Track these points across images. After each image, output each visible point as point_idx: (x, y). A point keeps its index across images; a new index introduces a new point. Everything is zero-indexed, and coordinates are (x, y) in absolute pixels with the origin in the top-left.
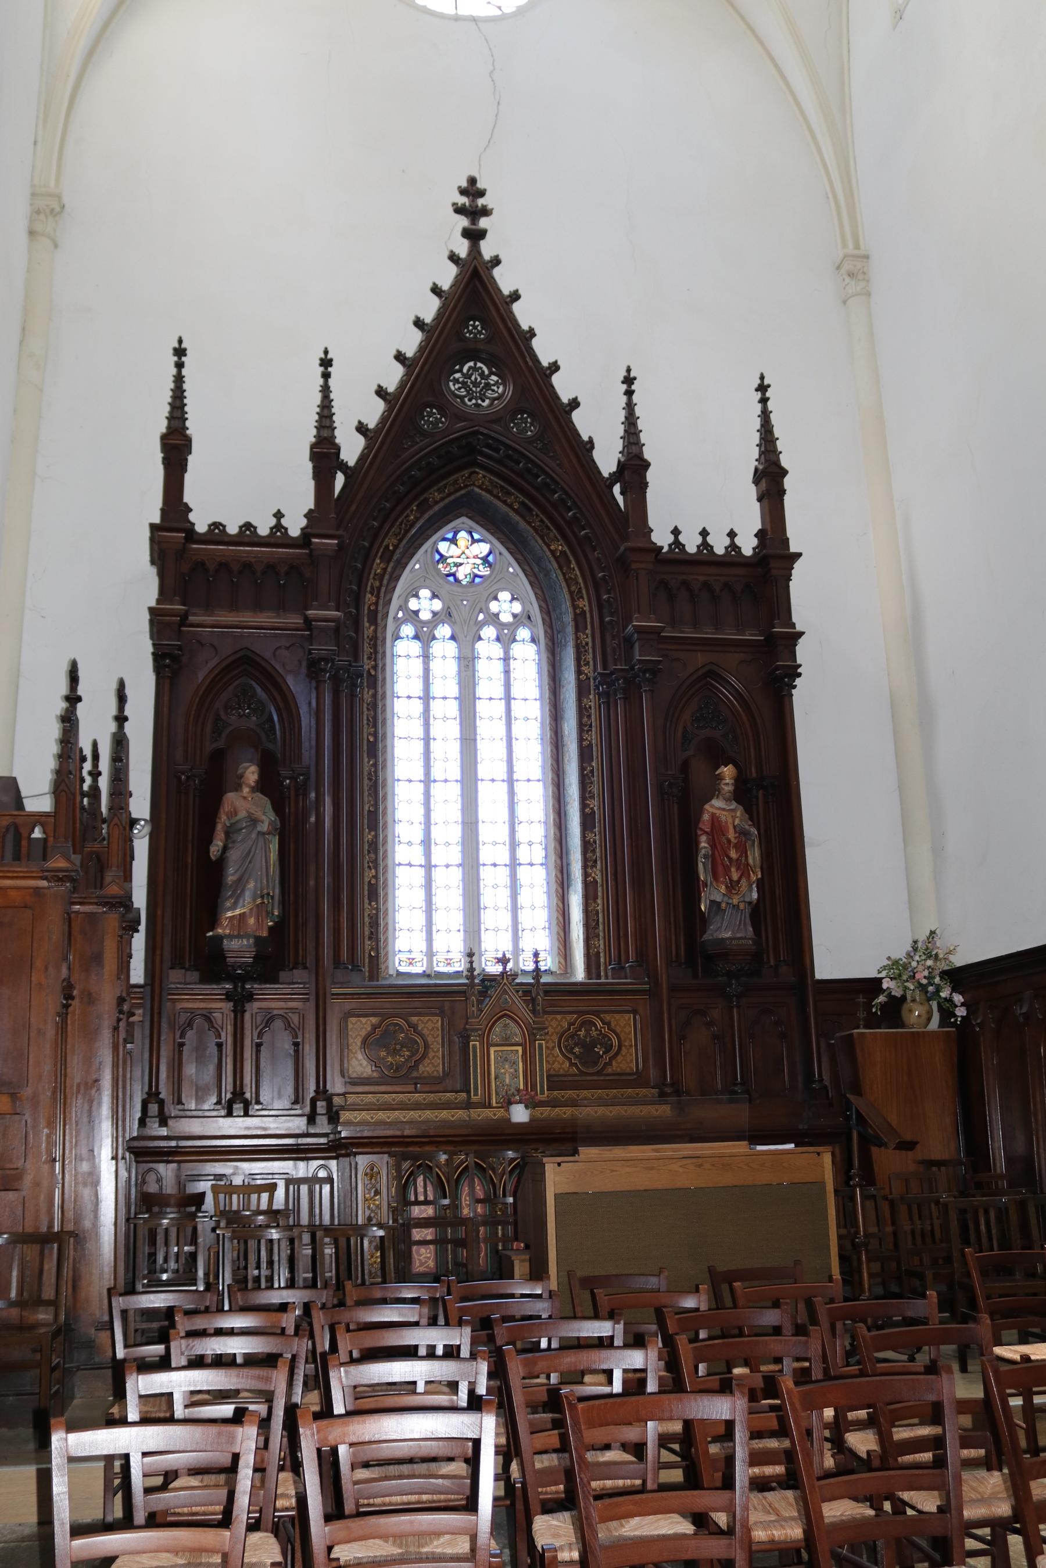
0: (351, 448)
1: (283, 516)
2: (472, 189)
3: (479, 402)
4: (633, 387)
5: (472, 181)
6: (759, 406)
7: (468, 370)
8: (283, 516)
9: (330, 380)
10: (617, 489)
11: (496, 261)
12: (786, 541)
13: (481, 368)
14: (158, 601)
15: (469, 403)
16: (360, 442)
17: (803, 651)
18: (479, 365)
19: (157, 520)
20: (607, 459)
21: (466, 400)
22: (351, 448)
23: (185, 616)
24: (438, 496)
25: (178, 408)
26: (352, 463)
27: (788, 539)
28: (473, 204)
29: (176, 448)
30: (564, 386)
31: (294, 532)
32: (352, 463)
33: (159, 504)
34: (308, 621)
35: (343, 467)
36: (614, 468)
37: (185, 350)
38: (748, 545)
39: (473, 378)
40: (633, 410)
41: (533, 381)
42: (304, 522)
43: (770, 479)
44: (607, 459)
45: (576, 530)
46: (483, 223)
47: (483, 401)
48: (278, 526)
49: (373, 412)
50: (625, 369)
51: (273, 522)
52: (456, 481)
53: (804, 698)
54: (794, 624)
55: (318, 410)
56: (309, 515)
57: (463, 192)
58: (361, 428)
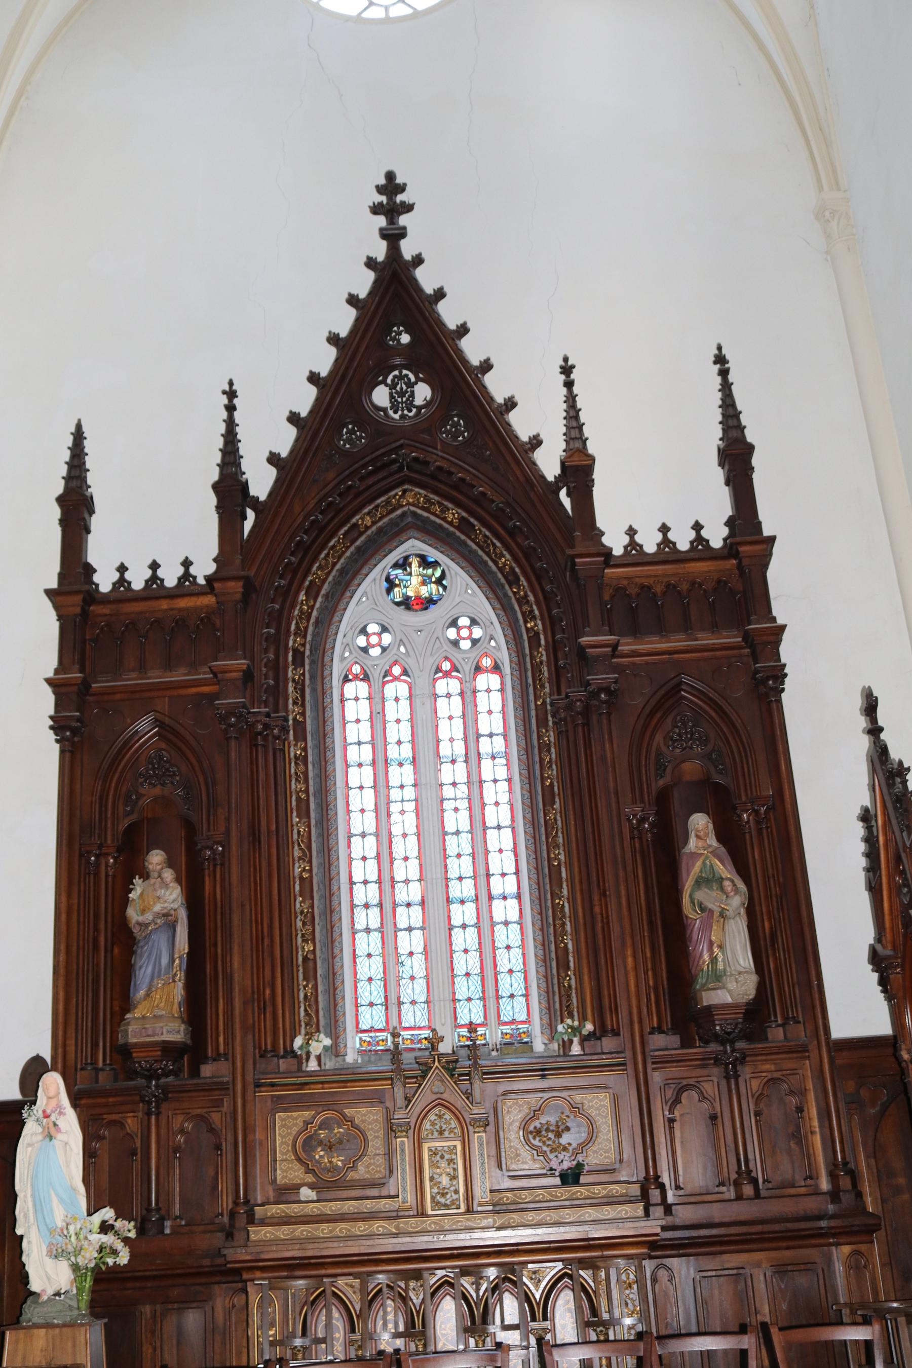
0: (261, 481)
1: (127, 569)
2: (391, 186)
3: (406, 412)
4: (572, 376)
5: (390, 176)
6: (564, 391)
7: (393, 381)
8: (127, 569)
9: (236, 413)
10: (563, 494)
11: (418, 260)
12: (758, 526)
13: (407, 376)
14: (57, 672)
15: (411, 414)
16: (271, 473)
17: (787, 651)
18: (405, 372)
19: (54, 584)
20: (549, 462)
21: (391, 412)
22: (261, 481)
23: (615, 647)
24: (368, 521)
25: (230, 453)
26: (263, 497)
27: (760, 523)
28: (391, 201)
29: (76, 507)
30: (497, 386)
31: (716, 543)
32: (263, 497)
33: (57, 568)
34: (746, 636)
35: (255, 503)
36: (557, 471)
37: (235, 392)
38: (716, 535)
39: (398, 388)
40: (574, 401)
41: (460, 385)
42: (725, 531)
43: (736, 457)
44: (549, 462)
45: (520, 540)
46: (403, 220)
47: (410, 411)
48: (666, 541)
49: (284, 440)
50: (715, 346)
51: (692, 535)
52: (388, 502)
53: (792, 700)
54: (775, 618)
55: (565, 422)
56: (730, 523)
57: (380, 190)
58: (273, 459)
